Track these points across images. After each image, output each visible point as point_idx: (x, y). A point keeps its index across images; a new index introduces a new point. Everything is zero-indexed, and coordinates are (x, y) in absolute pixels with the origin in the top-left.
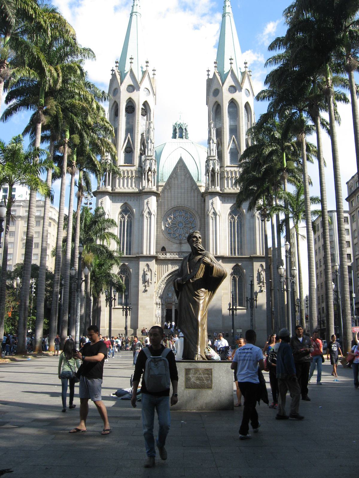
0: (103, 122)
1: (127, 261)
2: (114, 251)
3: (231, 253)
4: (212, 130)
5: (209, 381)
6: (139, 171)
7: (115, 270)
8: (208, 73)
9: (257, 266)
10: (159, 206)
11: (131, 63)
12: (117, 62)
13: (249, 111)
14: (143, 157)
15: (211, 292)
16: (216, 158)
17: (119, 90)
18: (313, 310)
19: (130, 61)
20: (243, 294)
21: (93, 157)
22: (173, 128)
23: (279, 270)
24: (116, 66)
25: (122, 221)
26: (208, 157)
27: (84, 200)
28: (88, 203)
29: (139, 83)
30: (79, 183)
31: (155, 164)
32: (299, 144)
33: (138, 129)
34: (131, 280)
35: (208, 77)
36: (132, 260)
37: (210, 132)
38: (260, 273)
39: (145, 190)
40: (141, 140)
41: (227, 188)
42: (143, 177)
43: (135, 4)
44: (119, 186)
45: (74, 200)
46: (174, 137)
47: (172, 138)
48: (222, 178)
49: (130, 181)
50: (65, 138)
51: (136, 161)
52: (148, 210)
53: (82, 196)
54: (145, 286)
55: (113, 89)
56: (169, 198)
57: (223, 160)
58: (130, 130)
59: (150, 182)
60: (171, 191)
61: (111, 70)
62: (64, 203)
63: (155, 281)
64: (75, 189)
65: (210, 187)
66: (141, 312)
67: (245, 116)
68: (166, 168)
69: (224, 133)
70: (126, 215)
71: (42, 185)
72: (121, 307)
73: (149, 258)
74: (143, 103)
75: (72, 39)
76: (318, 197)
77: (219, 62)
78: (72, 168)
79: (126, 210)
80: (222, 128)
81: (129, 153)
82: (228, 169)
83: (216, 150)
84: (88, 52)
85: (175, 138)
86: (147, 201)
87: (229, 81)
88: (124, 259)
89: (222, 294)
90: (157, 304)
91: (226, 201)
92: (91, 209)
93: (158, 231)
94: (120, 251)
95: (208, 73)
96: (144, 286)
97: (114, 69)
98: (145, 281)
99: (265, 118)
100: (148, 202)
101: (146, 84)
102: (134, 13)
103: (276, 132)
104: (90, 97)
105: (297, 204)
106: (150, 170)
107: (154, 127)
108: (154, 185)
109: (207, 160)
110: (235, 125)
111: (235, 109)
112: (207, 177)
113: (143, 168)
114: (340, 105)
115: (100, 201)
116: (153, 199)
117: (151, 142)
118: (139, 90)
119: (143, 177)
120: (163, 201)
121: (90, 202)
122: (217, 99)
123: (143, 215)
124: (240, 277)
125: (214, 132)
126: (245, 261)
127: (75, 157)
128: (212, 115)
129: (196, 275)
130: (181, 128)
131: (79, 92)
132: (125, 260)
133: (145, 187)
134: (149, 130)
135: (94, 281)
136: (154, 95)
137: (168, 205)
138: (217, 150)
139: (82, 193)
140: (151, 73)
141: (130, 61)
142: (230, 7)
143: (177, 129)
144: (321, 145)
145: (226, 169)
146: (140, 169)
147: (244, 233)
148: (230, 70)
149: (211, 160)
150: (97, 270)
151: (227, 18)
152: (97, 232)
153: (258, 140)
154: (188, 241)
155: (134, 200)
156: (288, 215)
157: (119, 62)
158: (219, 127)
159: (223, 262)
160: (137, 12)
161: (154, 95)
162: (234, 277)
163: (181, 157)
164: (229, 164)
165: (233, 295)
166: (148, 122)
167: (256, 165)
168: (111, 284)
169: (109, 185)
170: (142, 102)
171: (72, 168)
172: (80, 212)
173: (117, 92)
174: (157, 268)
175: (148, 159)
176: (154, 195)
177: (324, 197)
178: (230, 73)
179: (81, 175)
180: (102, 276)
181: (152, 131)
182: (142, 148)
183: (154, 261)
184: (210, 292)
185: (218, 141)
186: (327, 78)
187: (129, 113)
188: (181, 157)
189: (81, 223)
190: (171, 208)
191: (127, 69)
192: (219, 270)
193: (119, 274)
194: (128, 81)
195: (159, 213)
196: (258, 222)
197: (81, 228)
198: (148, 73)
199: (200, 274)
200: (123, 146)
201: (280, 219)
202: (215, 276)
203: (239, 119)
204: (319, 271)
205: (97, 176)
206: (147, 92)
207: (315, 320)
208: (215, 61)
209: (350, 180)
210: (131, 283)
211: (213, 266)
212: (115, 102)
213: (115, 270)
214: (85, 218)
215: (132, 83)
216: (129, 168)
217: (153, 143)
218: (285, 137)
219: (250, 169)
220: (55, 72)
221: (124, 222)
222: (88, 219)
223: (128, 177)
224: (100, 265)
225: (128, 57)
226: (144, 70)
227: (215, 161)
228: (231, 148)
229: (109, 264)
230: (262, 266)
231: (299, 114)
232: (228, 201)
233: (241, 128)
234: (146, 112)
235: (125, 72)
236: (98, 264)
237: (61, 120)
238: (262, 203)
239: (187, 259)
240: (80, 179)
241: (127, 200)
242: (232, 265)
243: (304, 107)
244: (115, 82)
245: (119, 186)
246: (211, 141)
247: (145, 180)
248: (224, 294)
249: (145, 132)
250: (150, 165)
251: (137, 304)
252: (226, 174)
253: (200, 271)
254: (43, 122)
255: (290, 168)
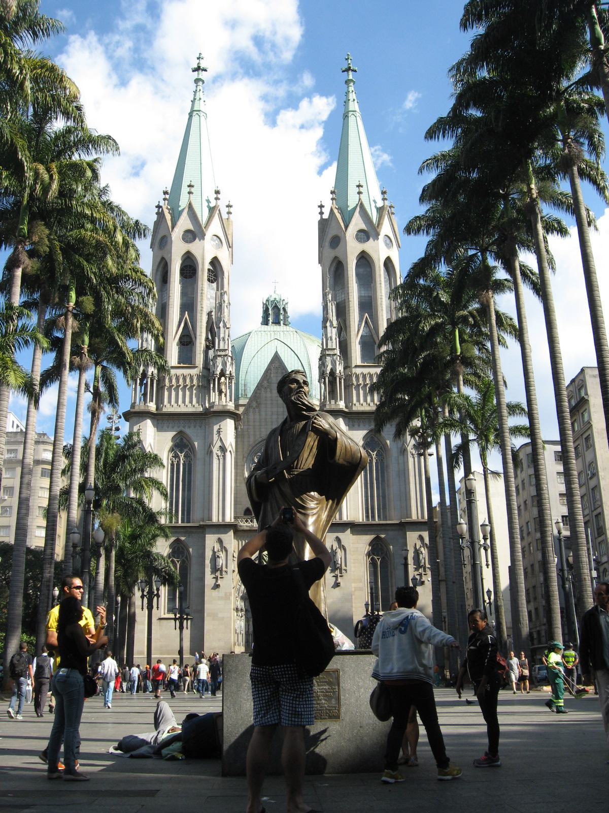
0: (136, 273)
1: (184, 534)
2: (160, 513)
3: (367, 517)
4: (329, 304)
5: (333, 701)
6: (203, 376)
7: (162, 547)
8: (321, 210)
9: (412, 538)
10: (239, 435)
11: (190, 193)
12: (165, 193)
13: (392, 272)
14: (211, 353)
15: (333, 500)
16: (338, 352)
17: (169, 241)
18: (520, 605)
19: (188, 189)
20: (390, 588)
21: (118, 340)
22: (263, 308)
23: (458, 526)
24: (165, 199)
25: (175, 463)
26: (323, 350)
27: (103, 418)
28: (114, 429)
29: (203, 226)
30: (94, 386)
31: (232, 364)
32: (485, 310)
33: (202, 304)
34: (190, 567)
35: (321, 217)
36: (192, 532)
37: (325, 308)
38: (419, 550)
39: (215, 409)
40: (207, 323)
41: (357, 404)
42: (212, 386)
43: (197, 98)
44: (170, 402)
45: (85, 417)
46: (265, 322)
47: (262, 324)
48: (348, 386)
49: (188, 393)
50: (68, 302)
51: (199, 360)
52: (219, 444)
53: (100, 410)
54: (216, 578)
55: (159, 236)
56: (257, 424)
57: (349, 356)
58: (189, 305)
59: (223, 395)
60: (259, 412)
61: (156, 207)
62: (64, 417)
63: (233, 568)
64: (87, 397)
65: (328, 403)
66: (209, 625)
67: (385, 282)
68: (253, 370)
69: (349, 310)
70: (181, 453)
71: (14, 370)
72: (172, 616)
73: (223, 527)
74: (209, 261)
75: (74, 109)
76: (518, 403)
77: (339, 192)
78: (81, 359)
79: (181, 444)
80: (347, 301)
81: (187, 345)
82: (358, 371)
83: (336, 339)
84: (106, 142)
85: (267, 324)
86: (218, 427)
87: (357, 223)
88: (178, 530)
89: (353, 589)
90: (237, 610)
91: (356, 426)
92: (118, 438)
93: (238, 481)
94: (171, 514)
95: (321, 210)
96: (214, 578)
97: (160, 205)
98: (215, 569)
99: (421, 268)
100: (220, 429)
101: (215, 228)
102: (195, 113)
103: (441, 292)
104: (111, 223)
105: (483, 415)
106: (223, 374)
107: (229, 300)
108: (231, 400)
109: (321, 357)
110: (368, 296)
111: (368, 269)
112: (323, 385)
113: (211, 371)
114: (554, 242)
115: (135, 429)
116: (229, 424)
117: (225, 326)
118: (204, 239)
119: (212, 386)
120: (246, 427)
121: (117, 426)
122: (338, 252)
123: (211, 452)
124: (383, 559)
125: (332, 309)
126: (392, 530)
127: (87, 339)
128: (328, 280)
129: (298, 458)
130: (276, 308)
131: (92, 214)
132: (179, 533)
133: (214, 403)
134: (221, 306)
135: (123, 566)
136: (230, 246)
137: (255, 435)
138: (338, 339)
139: (99, 405)
140: (224, 211)
141: (188, 189)
142: (356, 101)
143: (270, 309)
144: (522, 306)
145: (354, 370)
146: (206, 372)
147: (388, 481)
148: (357, 205)
149: (329, 355)
150: (127, 545)
151: (352, 119)
152: (126, 475)
153: (409, 307)
154: (280, 390)
155: (195, 427)
156: (467, 436)
157: (169, 192)
158: (340, 300)
159: (353, 533)
160: (199, 111)
161: (230, 247)
162: (373, 559)
163: (277, 352)
164: (359, 363)
165: (371, 589)
166: (219, 293)
167: (405, 354)
168: (151, 570)
169: (151, 400)
170: (208, 260)
171: (81, 359)
172: (96, 441)
173: (166, 242)
174: (237, 546)
175: (220, 356)
176: (231, 418)
177: (533, 397)
178: (358, 209)
179: (97, 373)
180: (136, 557)
181: (225, 307)
182: (210, 337)
183: (231, 533)
184: (331, 502)
185: (339, 324)
186: (529, 185)
187: (186, 278)
188: (277, 352)
189: (97, 459)
190: (260, 440)
191: (183, 203)
192: (349, 447)
193: (169, 556)
194: (184, 223)
195: (240, 450)
196: (411, 462)
197: (97, 468)
198: (219, 210)
199: (307, 459)
200: (175, 337)
201: (453, 445)
202: (341, 461)
203: (376, 285)
204: (526, 543)
205: (125, 372)
206: (217, 241)
207: (524, 622)
208: (333, 189)
209: (577, 377)
210: (190, 574)
211: (336, 439)
212: (163, 259)
213: (162, 547)
214: (106, 450)
215: (191, 227)
216: (186, 372)
217: (227, 328)
218: (458, 300)
219: (396, 361)
220: (46, 172)
221: (178, 465)
222: (111, 453)
223: (185, 386)
224: (134, 538)
225: (185, 183)
226: (212, 205)
227: (335, 357)
228: (362, 336)
229: (150, 536)
230: (421, 538)
231: (480, 258)
232: (359, 426)
233: (379, 301)
234: (215, 276)
235: (180, 209)
236: (130, 535)
237: (59, 265)
238: (419, 424)
239: (278, 432)
240: (96, 378)
241: (184, 427)
242: (369, 538)
243: (490, 245)
244: (162, 226)
245: (170, 402)
246: (328, 324)
247: (214, 391)
248: (355, 591)
249: (214, 310)
250: (222, 365)
251: (202, 611)
252: (354, 379)
253: (306, 453)
254: (25, 265)
255: (468, 355)
